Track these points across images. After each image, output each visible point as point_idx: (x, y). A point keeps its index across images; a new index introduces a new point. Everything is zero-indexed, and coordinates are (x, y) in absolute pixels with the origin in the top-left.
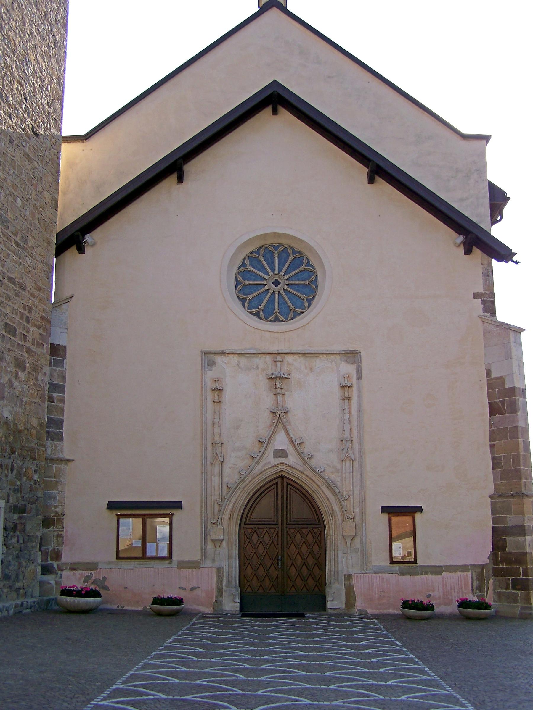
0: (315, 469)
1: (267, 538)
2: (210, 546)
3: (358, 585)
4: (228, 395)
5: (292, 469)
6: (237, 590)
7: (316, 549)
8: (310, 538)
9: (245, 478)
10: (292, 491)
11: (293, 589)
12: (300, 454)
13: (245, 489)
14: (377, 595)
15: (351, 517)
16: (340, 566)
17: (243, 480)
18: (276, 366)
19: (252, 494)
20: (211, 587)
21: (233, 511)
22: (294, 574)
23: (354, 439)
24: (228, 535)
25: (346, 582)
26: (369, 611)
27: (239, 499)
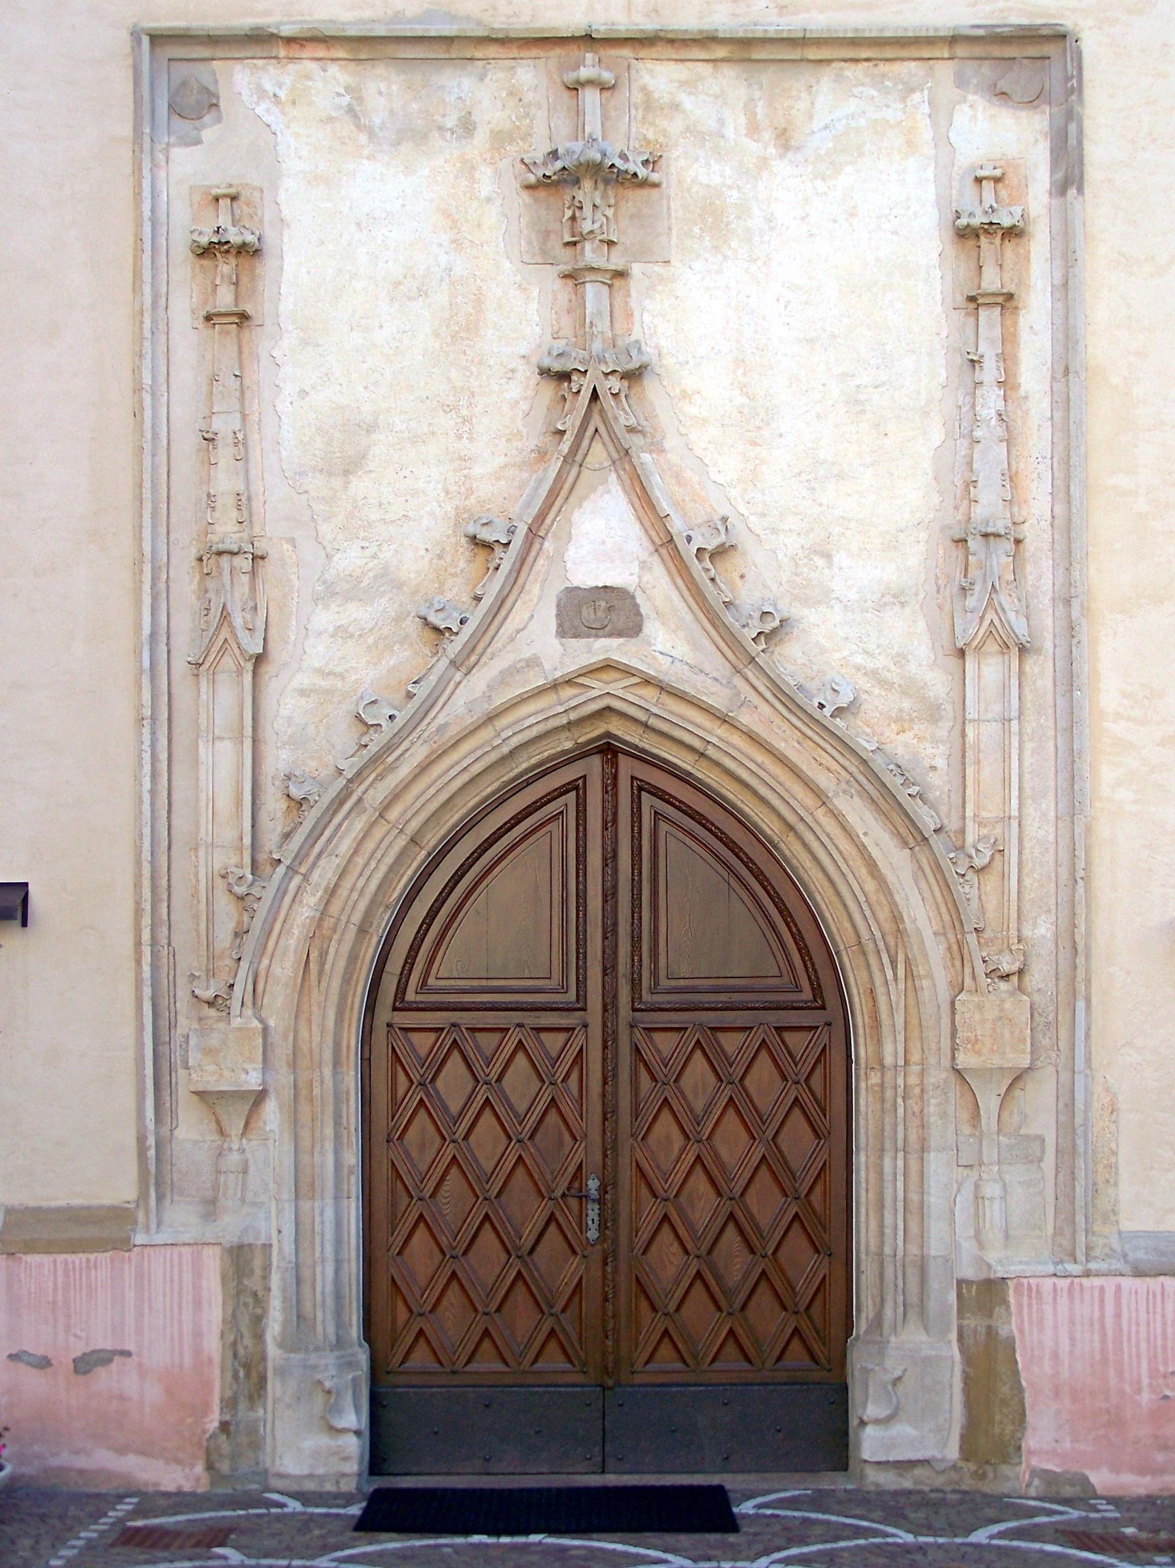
0: (800, 698)
1: (519, 1083)
2: (190, 1129)
3: (1049, 1337)
4: (295, 276)
5: (665, 698)
6: (351, 1365)
7: (798, 1141)
8: (763, 1080)
9: (388, 748)
10: (664, 827)
11: (666, 1350)
12: (712, 613)
13: (393, 814)
14: (1146, 1397)
15: (1007, 966)
16: (936, 1229)
17: (375, 760)
18: (578, 113)
19: (432, 840)
20: (197, 1352)
21: (318, 933)
22: (671, 1271)
23: (1026, 531)
24: (294, 1066)
25: (971, 1322)
26: (1101, 1479)
27: (360, 869)
